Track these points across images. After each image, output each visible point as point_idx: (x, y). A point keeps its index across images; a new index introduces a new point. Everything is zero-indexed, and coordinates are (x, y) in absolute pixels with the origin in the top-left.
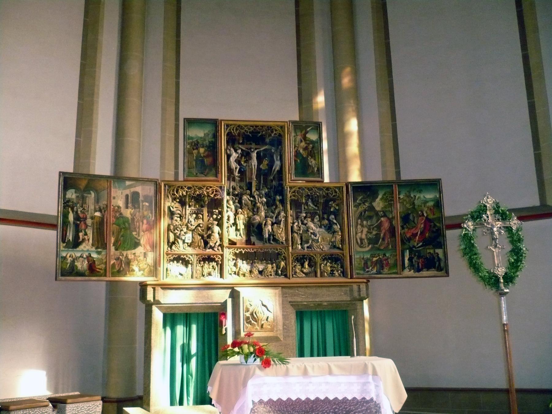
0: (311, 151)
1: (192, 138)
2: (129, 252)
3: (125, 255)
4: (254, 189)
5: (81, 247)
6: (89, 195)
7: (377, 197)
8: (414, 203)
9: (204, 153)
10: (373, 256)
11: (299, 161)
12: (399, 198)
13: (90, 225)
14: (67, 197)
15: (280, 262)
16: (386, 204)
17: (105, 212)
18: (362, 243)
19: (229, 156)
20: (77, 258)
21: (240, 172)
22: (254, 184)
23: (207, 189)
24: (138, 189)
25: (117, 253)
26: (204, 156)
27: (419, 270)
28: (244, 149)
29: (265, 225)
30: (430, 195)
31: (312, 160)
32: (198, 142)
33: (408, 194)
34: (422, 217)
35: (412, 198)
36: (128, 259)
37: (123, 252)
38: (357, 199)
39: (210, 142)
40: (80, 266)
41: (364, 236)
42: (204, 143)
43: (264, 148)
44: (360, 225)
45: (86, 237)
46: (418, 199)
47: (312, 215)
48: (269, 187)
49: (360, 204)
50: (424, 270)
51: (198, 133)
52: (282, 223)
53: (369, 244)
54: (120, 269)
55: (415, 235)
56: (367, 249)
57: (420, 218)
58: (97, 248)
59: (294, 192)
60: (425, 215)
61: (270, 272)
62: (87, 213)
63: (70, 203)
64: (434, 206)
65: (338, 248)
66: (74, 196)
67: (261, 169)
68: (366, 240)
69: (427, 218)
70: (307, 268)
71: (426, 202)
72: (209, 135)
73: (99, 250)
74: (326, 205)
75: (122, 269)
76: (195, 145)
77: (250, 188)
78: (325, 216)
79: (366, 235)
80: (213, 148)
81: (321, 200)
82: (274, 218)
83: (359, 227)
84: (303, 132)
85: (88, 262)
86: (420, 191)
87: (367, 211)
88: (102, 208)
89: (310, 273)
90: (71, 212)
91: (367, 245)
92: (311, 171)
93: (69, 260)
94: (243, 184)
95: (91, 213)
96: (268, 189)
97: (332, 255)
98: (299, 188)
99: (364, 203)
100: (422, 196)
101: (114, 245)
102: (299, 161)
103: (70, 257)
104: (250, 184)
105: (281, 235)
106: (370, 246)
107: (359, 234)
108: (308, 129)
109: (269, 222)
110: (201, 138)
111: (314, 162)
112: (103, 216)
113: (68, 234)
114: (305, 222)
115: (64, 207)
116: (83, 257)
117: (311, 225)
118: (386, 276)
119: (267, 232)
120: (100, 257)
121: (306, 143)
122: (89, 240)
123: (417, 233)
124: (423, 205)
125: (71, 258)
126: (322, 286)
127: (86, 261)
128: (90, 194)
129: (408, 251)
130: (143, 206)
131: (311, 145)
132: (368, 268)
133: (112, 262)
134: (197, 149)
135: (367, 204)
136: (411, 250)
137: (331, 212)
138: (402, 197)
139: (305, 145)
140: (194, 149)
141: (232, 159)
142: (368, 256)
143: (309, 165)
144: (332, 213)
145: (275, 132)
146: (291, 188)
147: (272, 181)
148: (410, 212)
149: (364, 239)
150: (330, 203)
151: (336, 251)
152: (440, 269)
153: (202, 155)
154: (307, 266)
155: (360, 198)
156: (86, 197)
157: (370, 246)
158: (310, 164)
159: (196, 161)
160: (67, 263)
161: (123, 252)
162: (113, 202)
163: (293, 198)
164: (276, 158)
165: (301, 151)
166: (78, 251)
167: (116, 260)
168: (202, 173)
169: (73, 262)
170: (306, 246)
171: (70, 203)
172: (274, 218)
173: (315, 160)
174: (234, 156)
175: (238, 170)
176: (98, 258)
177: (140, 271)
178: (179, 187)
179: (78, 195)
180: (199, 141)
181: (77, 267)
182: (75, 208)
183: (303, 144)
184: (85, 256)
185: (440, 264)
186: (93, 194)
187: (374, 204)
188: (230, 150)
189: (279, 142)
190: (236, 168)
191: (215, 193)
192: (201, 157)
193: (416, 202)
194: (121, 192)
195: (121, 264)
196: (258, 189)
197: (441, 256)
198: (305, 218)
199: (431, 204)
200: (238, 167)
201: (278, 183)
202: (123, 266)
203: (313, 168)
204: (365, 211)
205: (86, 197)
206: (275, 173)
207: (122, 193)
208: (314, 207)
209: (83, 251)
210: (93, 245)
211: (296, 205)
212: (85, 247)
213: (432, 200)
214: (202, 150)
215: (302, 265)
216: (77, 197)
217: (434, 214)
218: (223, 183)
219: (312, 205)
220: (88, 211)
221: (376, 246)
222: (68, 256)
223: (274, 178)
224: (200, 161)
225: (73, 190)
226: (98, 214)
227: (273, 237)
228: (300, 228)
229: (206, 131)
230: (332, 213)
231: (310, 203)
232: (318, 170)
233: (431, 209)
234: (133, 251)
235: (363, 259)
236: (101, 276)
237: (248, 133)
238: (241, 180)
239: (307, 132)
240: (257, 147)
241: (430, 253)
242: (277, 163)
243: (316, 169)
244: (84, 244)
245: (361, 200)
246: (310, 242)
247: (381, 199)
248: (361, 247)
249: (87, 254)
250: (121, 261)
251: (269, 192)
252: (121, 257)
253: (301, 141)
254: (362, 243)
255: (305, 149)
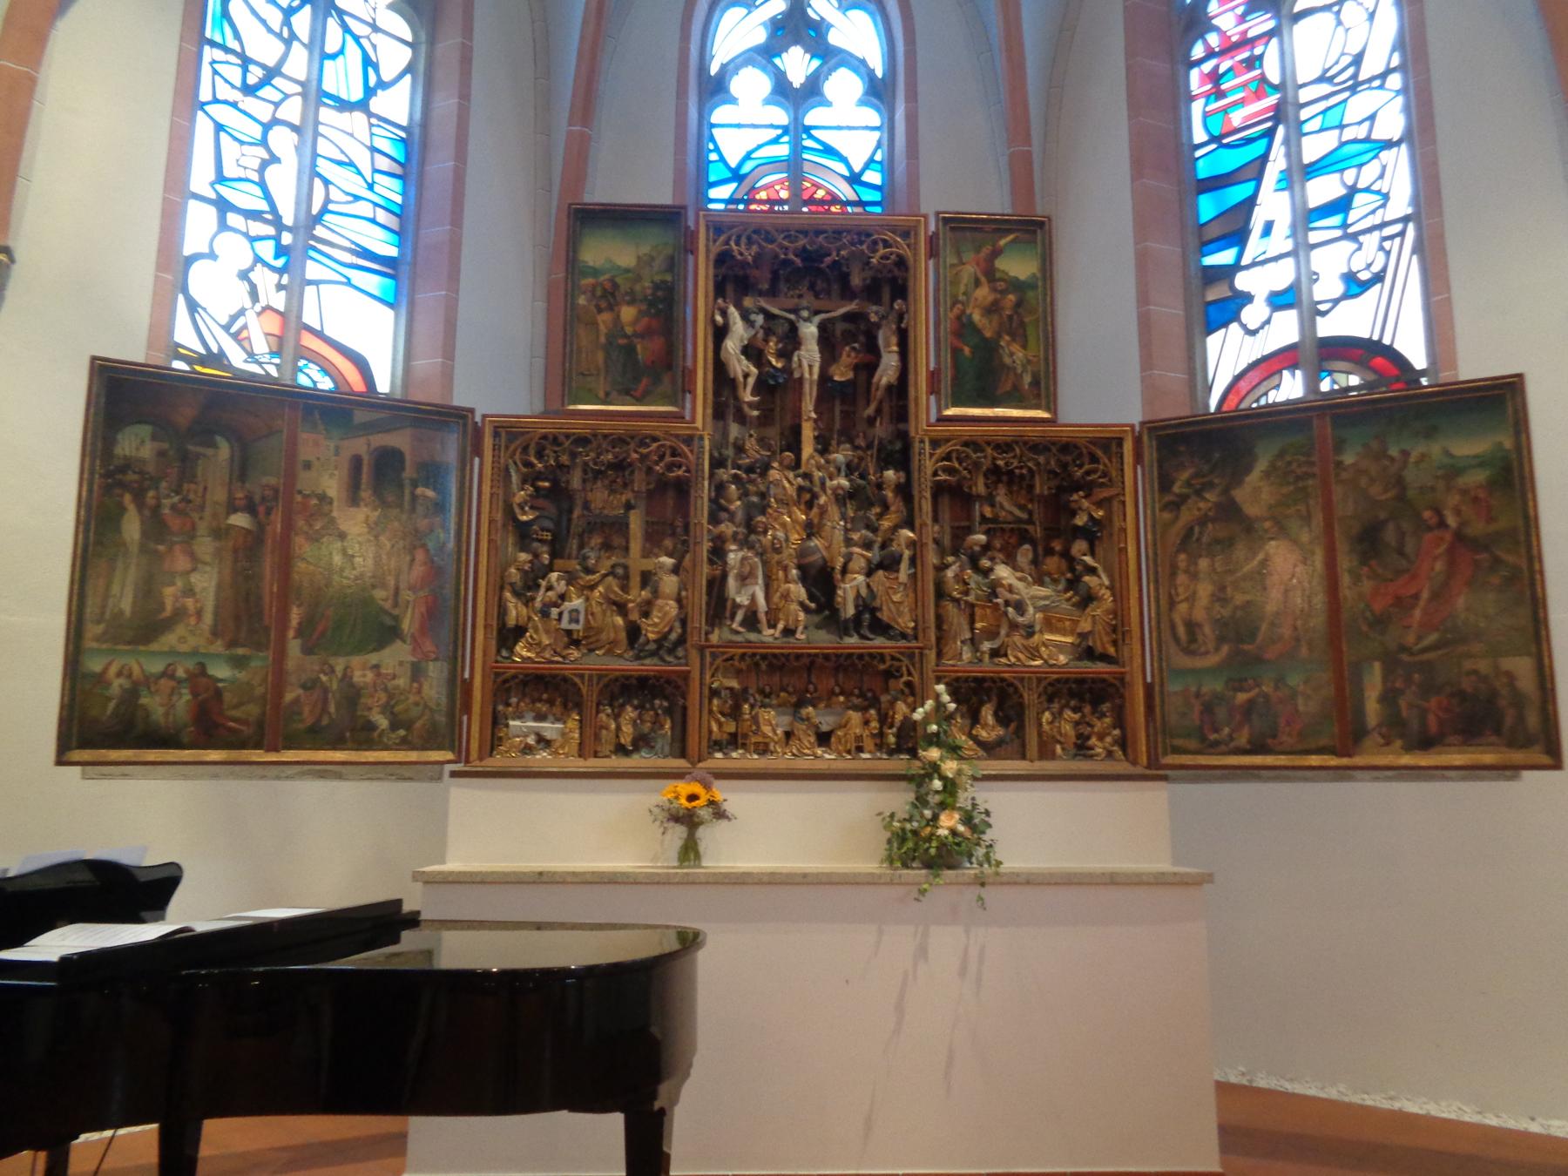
0: (1010, 317)
1: (595, 272)
2: (356, 660)
3: (339, 669)
4: (808, 449)
5: (169, 640)
6: (210, 452)
7: (1248, 469)
8: (1400, 482)
9: (636, 321)
10: (1238, 685)
11: (967, 350)
12: (1339, 464)
13: (208, 558)
14: (118, 451)
15: (892, 703)
16: (1285, 490)
17: (268, 512)
18: (1192, 637)
19: (720, 333)
20: (148, 681)
21: (761, 386)
22: (808, 433)
23: (642, 444)
24: (400, 440)
25: (313, 663)
26: (636, 335)
27: (1426, 743)
28: (776, 311)
29: (844, 571)
30: (1469, 446)
31: (1015, 348)
32: (615, 286)
33: (1375, 445)
34: (1437, 533)
35: (1392, 459)
36: (352, 685)
37: (332, 661)
38: (1173, 483)
39: (656, 287)
40: (160, 711)
41: (1199, 615)
42: (638, 288)
43: (842, 311)
44: (1186, 571)
45: (189, 602)
46: (1417, 463)
47: (1009, 538)
48: (861, 442)
49: (1183, 499)
50: (1451, 739)
51: (610, 253)
52: (904, 565)
53: (1221, 640)
54: (319, 719)
55: (1403, 604)
56: (1212, 660)
57: (1428, 536)
58: (232, 644)
59: (948, 457)
60: (1452, 521)
61: (859, 738)
62: (195, 516)
63: (131, 477)
64: (1491, 485)
65: (1105, 658)
66: (147, 451)
67: (830, 379)
68: (1207, 629)
69: (1459, 537)
70: (989, 730)
71: (1453, 471)
72: (653, 259)
73: (240, 651)
74: (1058, 508)
75: (325, 721)
76: (603, 296)
77: (794, 445)
78: (1057, 546)
79: (1208, 609)
80: (664, 305)
81: (1041, 487)
82: (876, 547)
83: (1182, 578)
84: (987, 250)
85: (195, 694)
86: (1430, 433)
87: (1213, 520)
88: (257, 498)
89: (1000, 742)
90: (132, 509)
91: (1211, 646)
92: (1008, 387)
93: (117, 685)
94: (773, 433)
95: (215, 515)
96: (856, 448)
97: (1081, 681)
98: (966, 444)
99: (1199, 493)
100: (1435, 449)
101: (300, 633)
102: (967, 350)
103: (119, 674)
104: (796, 431)
105: (897, 604)
106: (1225, 649)
107: (1183, 607)
108: (1002, 242)
109: (858, 563)
110: (627, 271)
111: (1020, 354)
112: (261, 527)
113: (115, 589)
114: (985, 563)
115: (107, 490)
116: (172, 677)
117: (1003, 572)
118: (1282, 760)
119: (851, 596)
120: (242, 675)
121: (994, 290)
122: (199, 614)
123: (1416, 597)
124: (1441, 485)
125: (121, 681)
126: (456, 633)
127: (185, 691)
128: (214, 445)
129: (1377, 666)
130: (414, 498)
131: (1011, 297)
132: (1216, 730)
133: (289, 697)
134: (611, 308)
135: (1211, 497)
136: (1391, 663)
137: (1077, 528)
138: (1349, 459)
139: (991, 298)
140: (600, 311)
141: (732, 345)
142: (1214, 685)
143: (1003, 365)
144: (1078, 532)
145: (882, 251)
146: (935, 443)
147: (871, 421)
148: (1382, 515)
149: (1199, 625)
150: (1075, 497)
151: (1101, 667)
152: (1518, 739)
153: (629, 330)
154: (990, 720)
155: (1185, 475)
156: (198, 456)
157: (1225, 649)
158: (1007, 360)
159: (609, 346)
160: (109, 699)
161: (332, 661)
162: (305, 481)
163: (943, 477)
164: (887, 340)
165: (976, 317)
166: (153, 653)
167: (304, 687)
168: (627, 392)
169: (132, 695)
170: (986, 646)
171: (131, 477)
172: (876, 547)
173: (1024, 347)
174: (739, 332)
175: (751, 381)
176: (233, 681)
177: (394, 726)
178: (544, 437)
179: (166, 446)
180: (619, 280)
181: (148, 714)
182: (151, 494)
183: (983, 293)
184: (180, 673)
185: (1521, 718)
186: (224, 450)
187: (1239, 494)
188: (724, 313)
189: (893, 283)
190: (746, 376)
191: (668, 459)
192: (626, 336)
193: (1410, 475)
194: (332, 445)
195: (325, 701)
196: (823, 447)
197: (1527, 683)
198: (986, 548)
199: (1478, 477)
200: (754, 371)
201: (891, 428)
202: (332, 709)
203: (1019, 377)
204: (1203, 521)
205: (198, 456)
206: (879, 394)
207: (337, 449)
208: (1018, 512)
209: (172, 652)
210: (215, 633)
211: (953, 494)
212: (182, 639)
213: (1481, 462)
214: (628, 313)
215: (975, 718)
216: (161, 454)
217: (1490, 519)
218: (699, 424)
219: (1007, 505)
220: (202, 508)
221: (1246, 647)
222: (113, 670)
223: (879, 411)
224: (622, 351)
225: (145, 430)
226: (240, 520)
227: (870, 618)
228: (966, 583)
229: (645, 249)
230: (1078, 532)
231: (1001, 496)
232: (1036, 383)
233: (1476, 500)
234: (374, 658)
235: (1198, 695)
236: (243, 746)
237: (791, 256)
238: (765, 420)
239: (996, 253)
240: (818, 304)
241: (1475, 672)
242: (889, 365)
243: (1027, 379)
244: (180, 630)
245: (1188, 484)
246: (1003, 632)
247: (1267, 474)
248: (1189, 652)
249: (190, 664)
250: (326, 691)
251: (861, 459)
252: (324, 678)
253: (977, 283)
254: (1192, 637)
255: (992, 309)
